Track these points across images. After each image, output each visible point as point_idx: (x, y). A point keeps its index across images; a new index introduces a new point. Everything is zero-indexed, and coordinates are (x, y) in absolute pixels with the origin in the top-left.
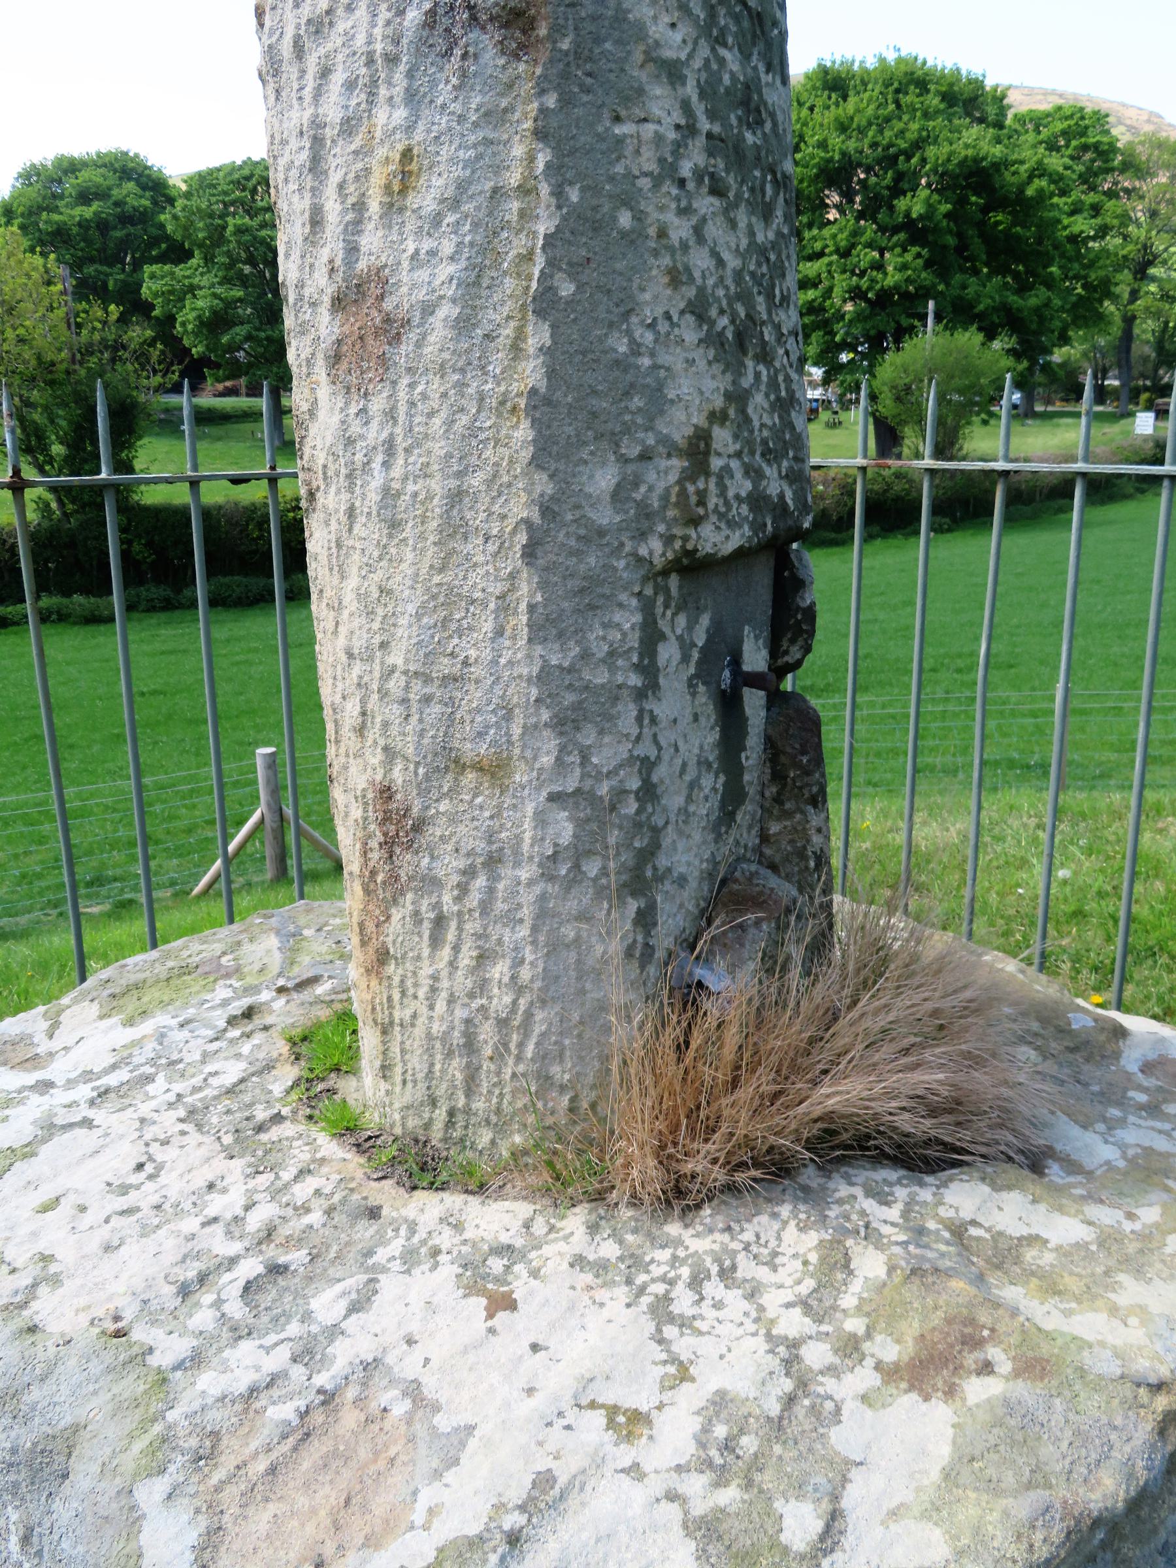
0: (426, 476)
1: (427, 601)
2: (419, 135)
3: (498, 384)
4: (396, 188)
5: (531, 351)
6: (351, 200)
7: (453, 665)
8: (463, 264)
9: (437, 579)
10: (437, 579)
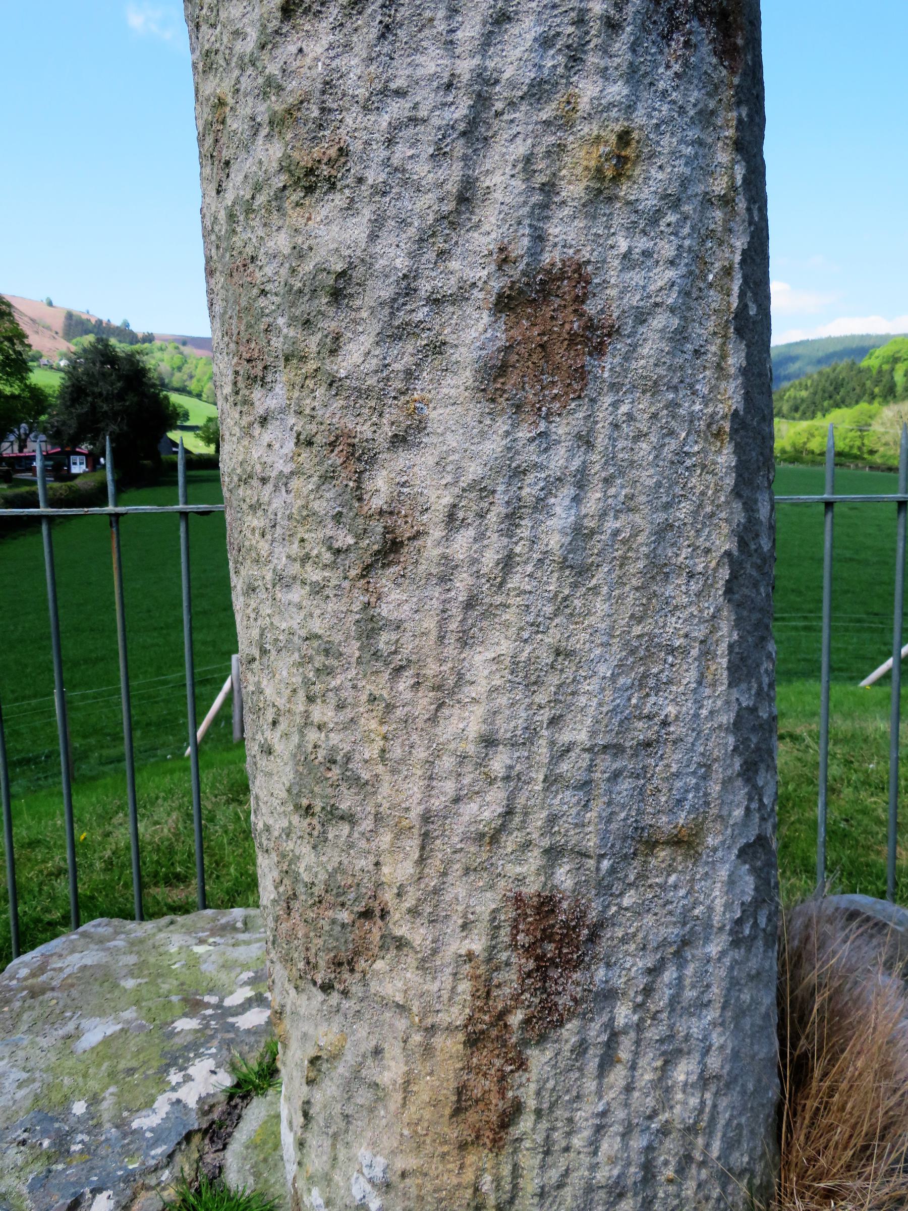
0: (630, 510)
1: (626, 658)
2: (640, 117)
3: (706, 406)
4: (609, 174)
5: (732, 371)
6: (540, 179)
7: (649, 728)
8: (683, 270)
9: (637, 630)
10: (637, 630)
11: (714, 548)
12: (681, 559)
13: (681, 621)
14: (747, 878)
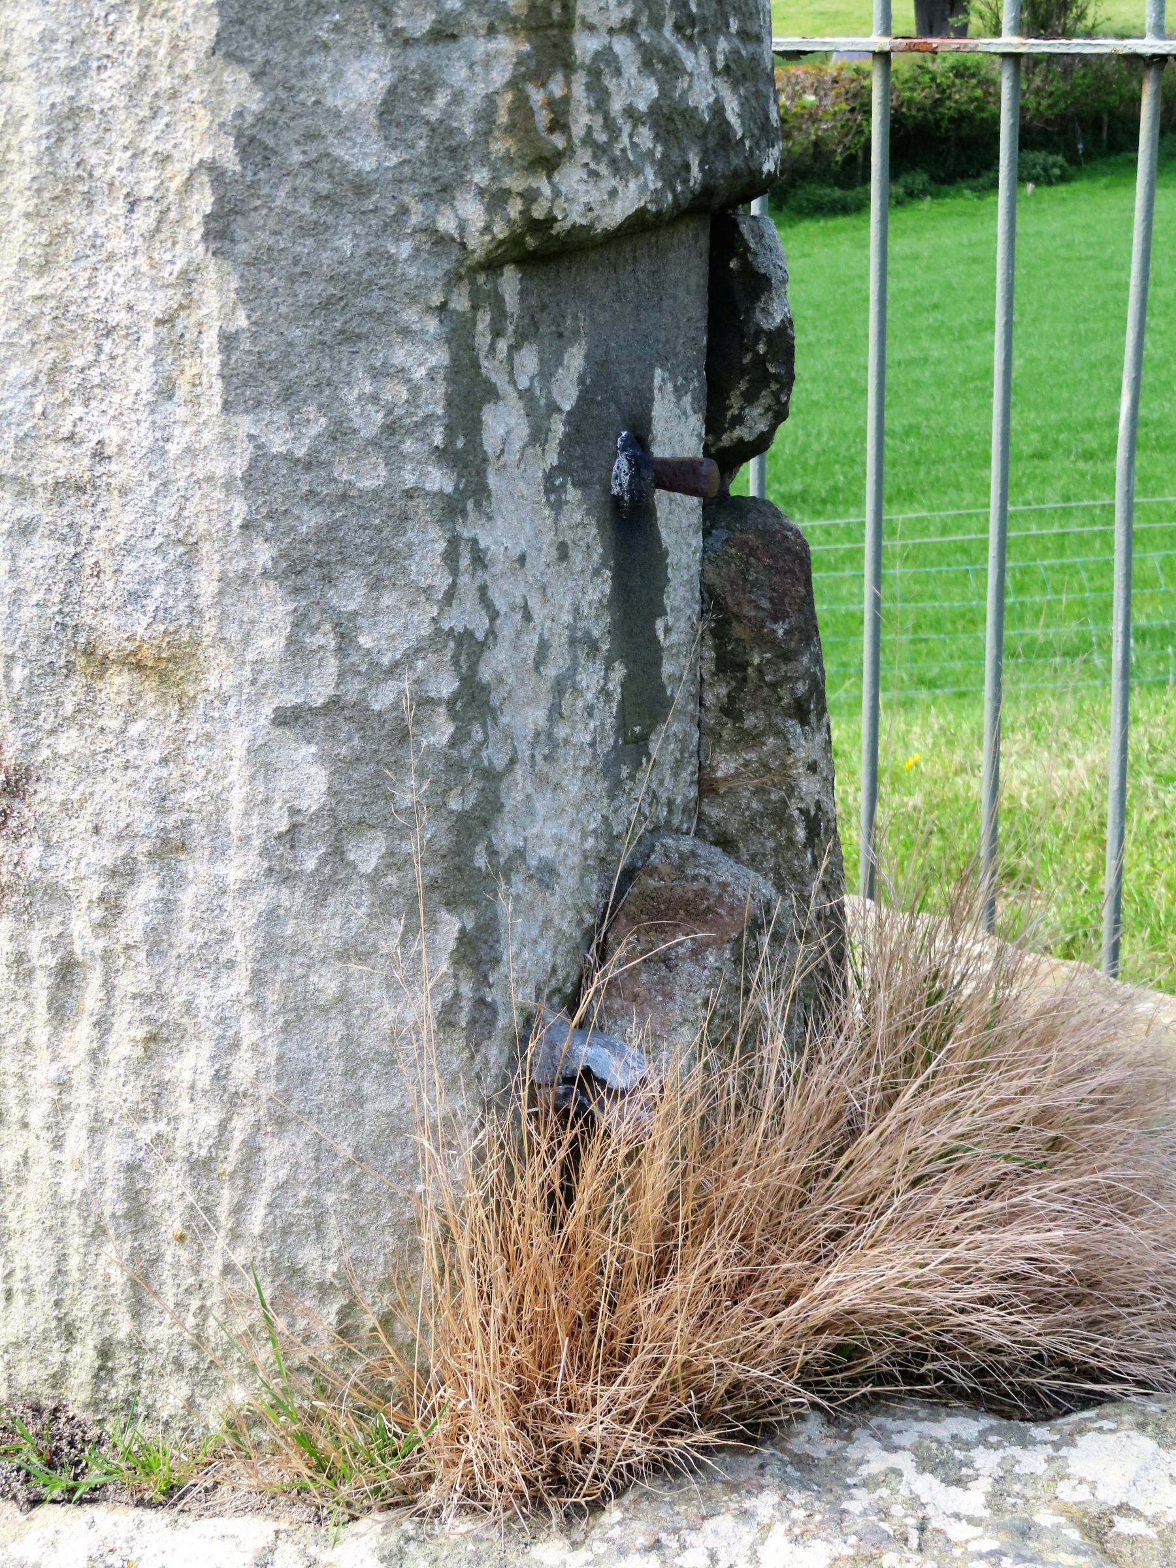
10: (34, 287)
11: (177, 155)
12: (112, 171)
13: (121, 281)
14: (313, 770)
